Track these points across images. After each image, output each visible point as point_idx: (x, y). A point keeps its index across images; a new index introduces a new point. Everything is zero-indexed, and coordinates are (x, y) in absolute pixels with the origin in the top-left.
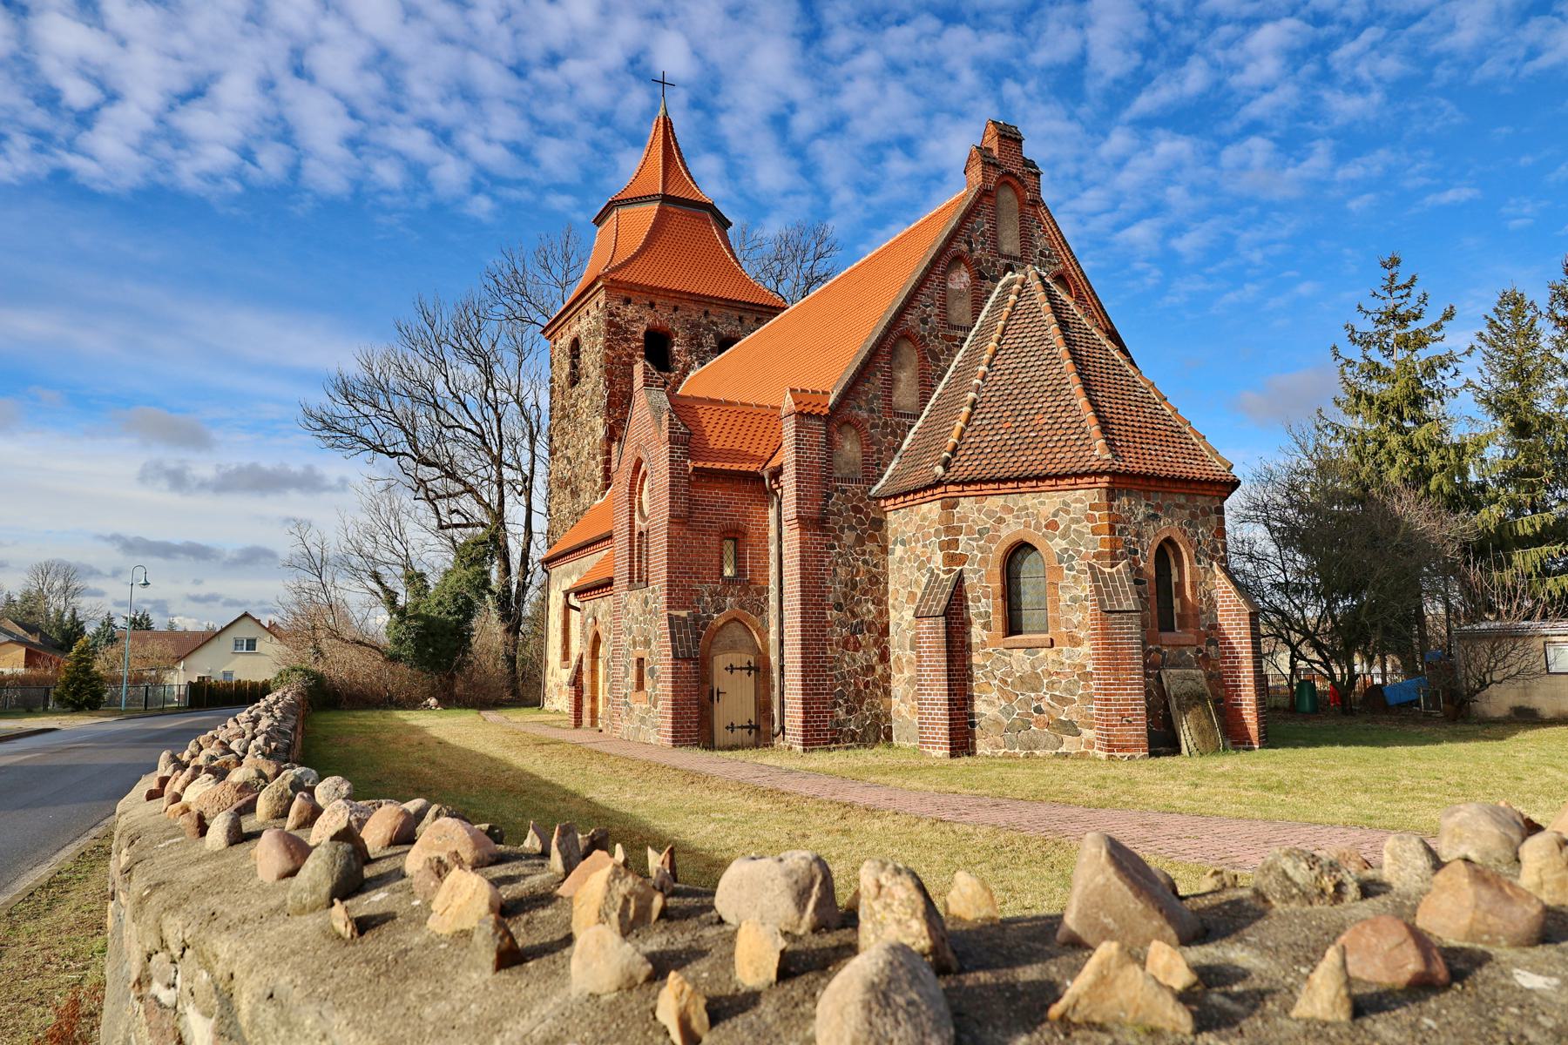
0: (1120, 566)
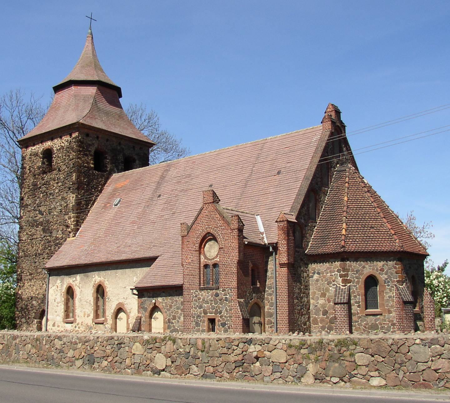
0: (404, 285)
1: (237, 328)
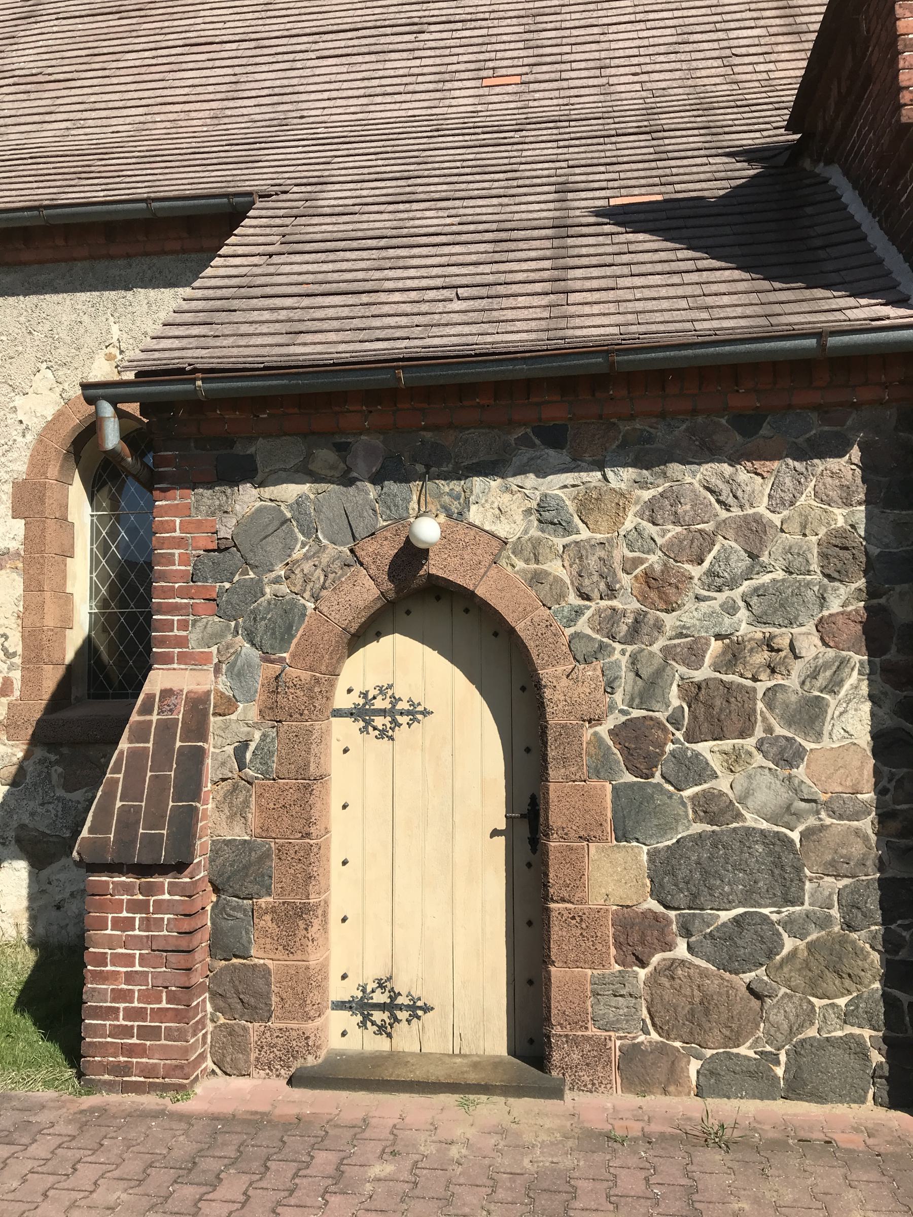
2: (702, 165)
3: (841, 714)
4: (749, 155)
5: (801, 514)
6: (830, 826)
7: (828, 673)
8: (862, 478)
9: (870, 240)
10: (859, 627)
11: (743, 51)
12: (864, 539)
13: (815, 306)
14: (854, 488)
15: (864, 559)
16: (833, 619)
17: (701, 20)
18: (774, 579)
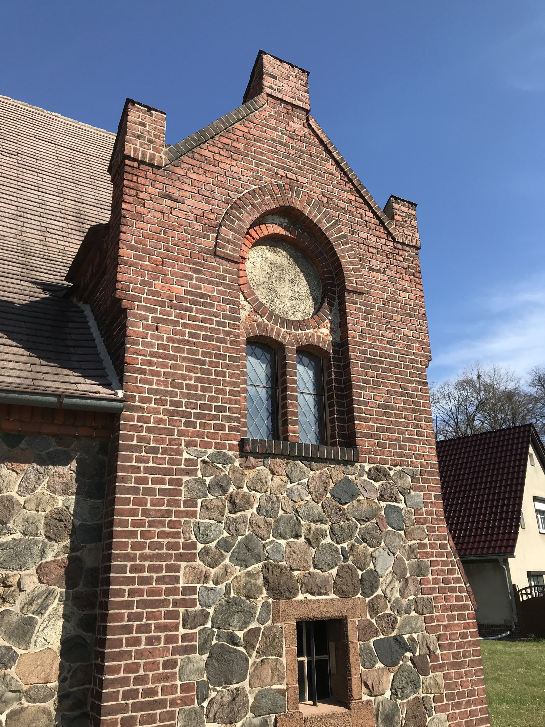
1: (460, 665)
2: (16, 284)
3: (44, 628)
4: (45, 286)
5: (37, 498)
6: (27, 708)
7: (40, 601)
8: (76, 479)
9: (98, 348)
10: (63, 570)
11: (53, 231)
12: (73, 515)
13: (61, 378)
14: (70, 485)
15: (71, 528)
16: (48, 565)
17: (33, 208)
18: (14, 539)
